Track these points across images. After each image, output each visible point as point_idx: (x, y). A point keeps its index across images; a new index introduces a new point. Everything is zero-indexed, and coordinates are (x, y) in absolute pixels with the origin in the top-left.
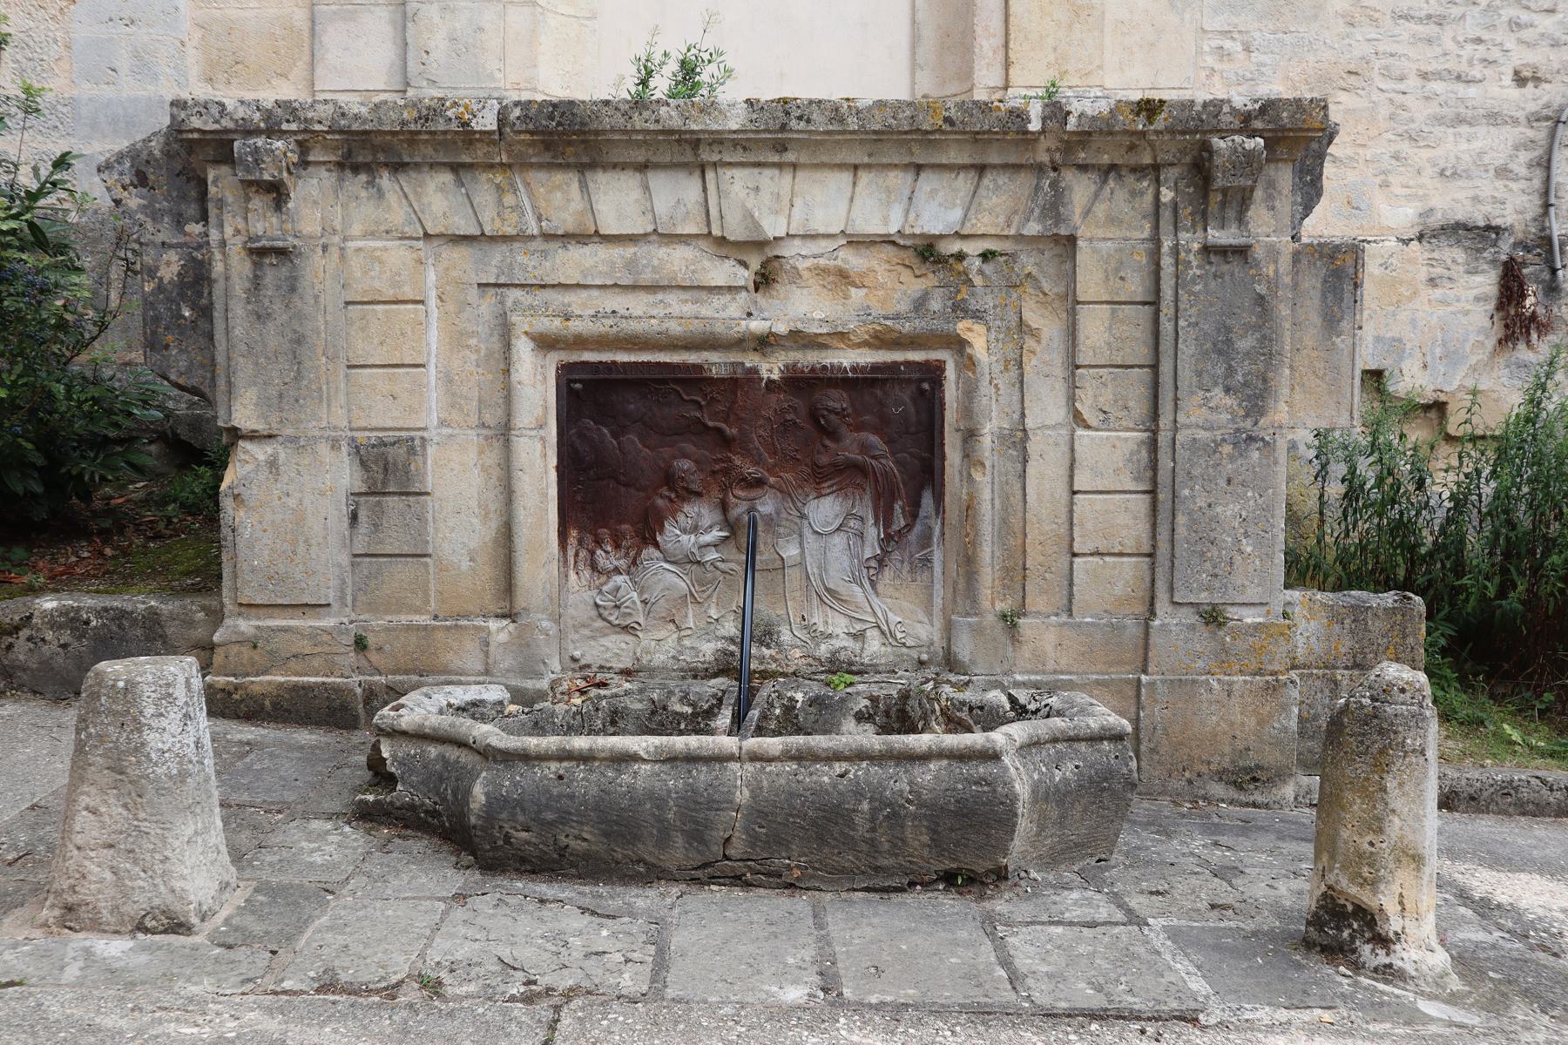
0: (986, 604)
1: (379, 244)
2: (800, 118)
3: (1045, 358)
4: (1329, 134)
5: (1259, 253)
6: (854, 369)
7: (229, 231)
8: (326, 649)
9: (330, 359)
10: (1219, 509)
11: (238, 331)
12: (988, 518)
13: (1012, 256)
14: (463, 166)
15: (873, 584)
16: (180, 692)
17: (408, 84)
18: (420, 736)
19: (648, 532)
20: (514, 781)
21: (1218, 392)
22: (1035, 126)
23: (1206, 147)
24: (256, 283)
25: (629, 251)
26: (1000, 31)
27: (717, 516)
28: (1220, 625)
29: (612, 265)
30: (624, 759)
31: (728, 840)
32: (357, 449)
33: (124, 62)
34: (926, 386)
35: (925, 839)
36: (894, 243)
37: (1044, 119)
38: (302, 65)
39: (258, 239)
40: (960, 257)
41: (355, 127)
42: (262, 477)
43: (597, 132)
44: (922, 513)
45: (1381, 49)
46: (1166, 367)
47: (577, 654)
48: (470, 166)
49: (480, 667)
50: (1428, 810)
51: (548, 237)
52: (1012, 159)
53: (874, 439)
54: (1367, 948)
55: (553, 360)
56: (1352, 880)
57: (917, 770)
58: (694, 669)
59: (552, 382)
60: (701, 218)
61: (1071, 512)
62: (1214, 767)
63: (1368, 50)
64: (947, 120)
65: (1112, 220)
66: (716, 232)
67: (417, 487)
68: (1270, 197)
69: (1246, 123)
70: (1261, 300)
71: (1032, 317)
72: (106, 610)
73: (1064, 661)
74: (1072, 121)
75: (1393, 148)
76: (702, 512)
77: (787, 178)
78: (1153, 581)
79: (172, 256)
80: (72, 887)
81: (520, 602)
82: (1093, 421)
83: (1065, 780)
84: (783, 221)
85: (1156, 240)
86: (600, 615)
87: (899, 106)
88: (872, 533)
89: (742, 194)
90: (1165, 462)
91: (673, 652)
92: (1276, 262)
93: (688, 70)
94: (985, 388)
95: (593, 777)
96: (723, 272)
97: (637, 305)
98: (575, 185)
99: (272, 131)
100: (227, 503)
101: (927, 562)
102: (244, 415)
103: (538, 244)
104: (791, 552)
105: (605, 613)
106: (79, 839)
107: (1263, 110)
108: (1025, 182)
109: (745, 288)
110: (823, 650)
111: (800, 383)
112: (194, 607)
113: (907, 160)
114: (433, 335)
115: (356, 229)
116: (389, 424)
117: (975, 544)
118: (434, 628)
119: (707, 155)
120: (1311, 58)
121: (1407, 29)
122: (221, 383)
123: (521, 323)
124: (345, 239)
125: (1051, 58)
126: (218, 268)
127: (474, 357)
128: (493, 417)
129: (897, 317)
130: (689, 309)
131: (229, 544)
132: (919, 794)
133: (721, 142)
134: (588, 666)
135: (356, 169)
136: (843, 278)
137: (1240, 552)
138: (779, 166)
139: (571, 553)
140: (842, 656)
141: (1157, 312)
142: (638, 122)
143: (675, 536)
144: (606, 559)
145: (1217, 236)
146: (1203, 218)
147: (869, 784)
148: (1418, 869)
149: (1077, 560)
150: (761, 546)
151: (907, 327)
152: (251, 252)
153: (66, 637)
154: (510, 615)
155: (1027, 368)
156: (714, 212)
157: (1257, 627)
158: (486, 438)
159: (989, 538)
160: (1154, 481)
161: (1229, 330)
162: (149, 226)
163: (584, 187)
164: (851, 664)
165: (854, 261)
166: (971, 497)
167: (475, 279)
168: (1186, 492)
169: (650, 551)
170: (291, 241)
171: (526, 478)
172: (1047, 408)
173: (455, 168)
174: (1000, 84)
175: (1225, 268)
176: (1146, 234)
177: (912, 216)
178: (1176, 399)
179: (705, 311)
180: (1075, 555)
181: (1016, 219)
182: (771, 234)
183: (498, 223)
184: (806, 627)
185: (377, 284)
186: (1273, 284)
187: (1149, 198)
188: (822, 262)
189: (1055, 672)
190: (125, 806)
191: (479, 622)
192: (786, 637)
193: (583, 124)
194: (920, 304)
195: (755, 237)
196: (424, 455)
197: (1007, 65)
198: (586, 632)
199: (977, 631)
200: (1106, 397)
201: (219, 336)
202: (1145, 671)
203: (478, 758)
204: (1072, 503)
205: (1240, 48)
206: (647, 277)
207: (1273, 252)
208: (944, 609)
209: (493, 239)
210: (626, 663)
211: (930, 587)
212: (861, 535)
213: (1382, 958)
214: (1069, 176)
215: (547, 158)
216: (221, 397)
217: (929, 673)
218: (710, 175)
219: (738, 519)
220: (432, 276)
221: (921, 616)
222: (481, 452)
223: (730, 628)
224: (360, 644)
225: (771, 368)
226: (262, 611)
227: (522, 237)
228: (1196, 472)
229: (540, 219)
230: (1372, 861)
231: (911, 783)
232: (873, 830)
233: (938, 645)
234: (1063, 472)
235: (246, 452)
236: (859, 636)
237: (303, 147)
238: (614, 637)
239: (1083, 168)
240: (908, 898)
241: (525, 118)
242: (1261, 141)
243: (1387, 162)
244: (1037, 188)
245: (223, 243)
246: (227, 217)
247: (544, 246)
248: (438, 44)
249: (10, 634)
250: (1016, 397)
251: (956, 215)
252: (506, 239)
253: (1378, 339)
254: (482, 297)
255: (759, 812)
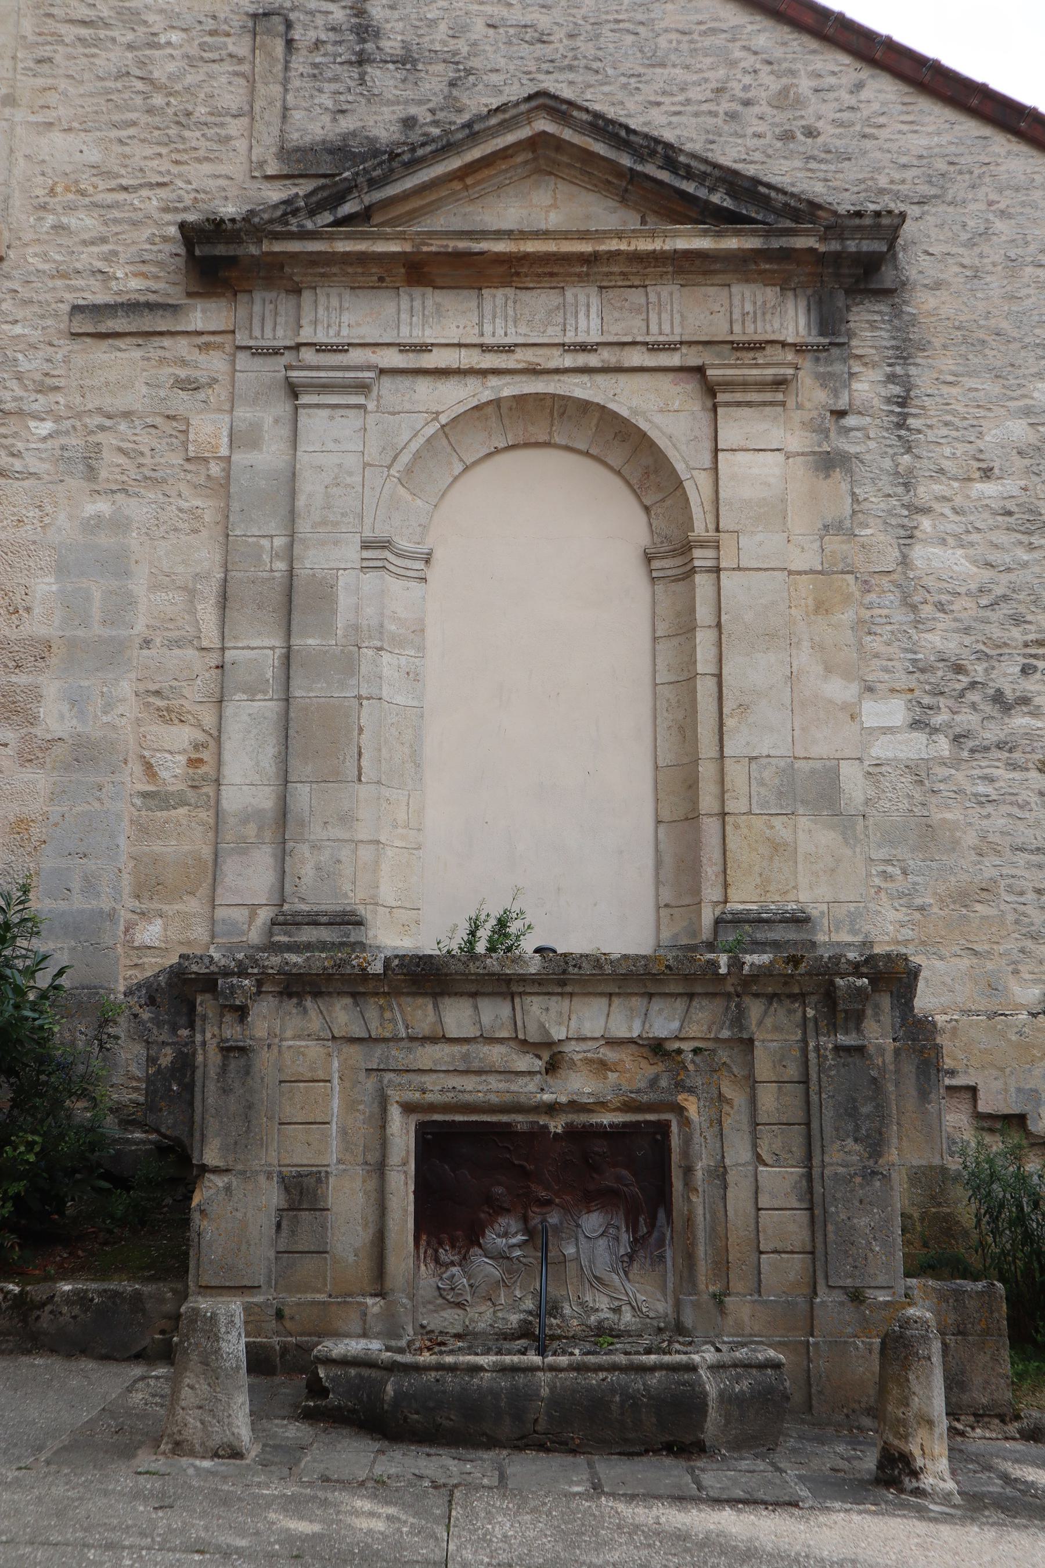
0: (702, 1287)
1: (303, 1043)
2: (575, 966)
3: (736, 1118)
4: (913, 974)
5: (872, 1050)
6: (611, 1125)
7: (208, 1035)
8: (257, 1318)
9: (270, 1119)
10: (855, 1221)
11: (210, 1101)
12: (701, 1226)
13: (714, 1051)
14: (359, 993)
15: (626, 1273)
16: (237, 1320)
17: (284, 901)
18: (345, 1362)
19: (473, 1237)
20: (407, 1383)
21: (850, 1141)
22: (723, 970)
23: (832, 983)
24: (224, 1069)
25: (465, 1048)
26: (720, 861)
27: (520, 1225)
28: (862, 1302)
29: (453, 1056)
30: (477, 1369)
31: (536, 1420)
32: (282, 1179)
33: (76, 885)
34: (659, 1137)
35: (654, 1420)
36: (635, 1043)
37: (729, 966)
38: (206, 885)
39: (228, 1040)
40: (679, 1051)
41: (294, 971)
42: (220, 1198)
43: (446, 975)
44: (658, 1224)
45: (1004, 872)
46: (815, 1125)
47: (425, 1322)
48: (364, 994)
49: (360, 1332)
50: (935, 1393)
51: (412, 1039)
52: (711, 990)
53: (625, 1172)
54: (907, 1479)
55: (413, 1120)
56: (895, 1436)
57: (648, 1376)
58: (505, 1334)
59: (412, 1134)
60: (511, 1027)
61: (757, 1223)
62: (863, 1405)
63: (994, 873)
64: (668, 967)
65: (776, 1029)
66: (521, 1036)
67: (322, 1205)
68: (876, 1014)
69: (856, 969)
70: (874, 1080)
71: (727, 1091)
72: (105, 1291)
73: (756, 1328)
74: (746, 968)
75: (1020, 945)
76: (510, 1223)
77: (566, 1002)
78: (815, 1271)
79: (168, 1050)
80: (180, 1432)
81: (389, 1284)
82: (769, 1161)
83: (742, 1391)
84: (564, 1029)
85: (805, 1041)
86: (441, 1295)
87: (637, 958)
88: (625, 1237)
89: (538, 1013)
90: (818, 1189)
91: (490, 1322)
92: (883, 1055)
93: (502, 923)
94: (697, 1139)
95: (456, 1380)
96: (524, 1062)
97: (469, 1083)
98: (430, 1006)
99: (242, 973)
100: (196, 1216)
101: (662, 1258)
102: (211, 1156)
103: (405, 1044)
104: (570, 1250)
105: (444, 1293)
106: (183, 1404)
107: (867, 961)
108: (718, 1004)
109: (539, 1072)
110: (593, 1319)
111: (576, 1134)
112: (166, 1290)
113: (643, 990)
114: (336, 1103)
115: (289, 1034)
116: (305, 1162)
117: (693, 1244)
118: (330, 1303)
119: (515, 988)
120: (953, 879)
121: (1022, 858)
122: (197, 1135)
123: (394, 1095)
124: (281, 1040)
125: (758, 881)
126: (200, 1058)
127: (362, 1117)
128: (373, 1157)
129: (638, 1091)
130: (502, 1086)
131: (195, 1244)
132: (649, 1391)
133: (525, 980)
134: (432, 1331)
135: (290, 995)
136: (602, 1066)
137: (872, 1250)
138: (561, 994)
139: (422, 1251)
140: (606, 1324)
141: (808, 1088)
142: (472, 968)
143: (493, 1239)
144: (445, 1255)
145: (843, 1039)
146: (833, 1028)
147: (619, 1385)
148: (931, 1429)
149: (763, 1256)
150: (550, 1246)
151: (645, 1098)
152: (222, 1049)
153: (76, 1310)
154: (381, 1294)
155: (725, 1125)
156: (519, 1024)
157: (887, 1304)
158: (368, 1172)
159: (702, 1240)
160: (811, 1201)
161: (854, 1100)
162: (155, 1031)
163: (436, 1007)
164: (612, 1329)
165: (610, 1055)
166: (690, 1212)
167: (364, 1066)
168: (833, 1209)
169: (476, 1250)
170: (249, 1042)
171: (394, 1199)
172: (738, 1152)
173: (354, 995)
174: (721, 899)
175: (850, 1060)
176: (799, 1037)
177: (647, 1026)
178: (823, 1146)
179: (514, 1087)
180: (761, 1253)
181: (714, 1028)
182: (556, 1038)
183: (380, 1030)
184: (581, 1304)
185: (301, 1069)
186: (883, 1070)
187: (799, 1014)
188: (589, 1055)
189: (751, 1335)
190: (209, 1384)
191: (360, 1299)
192: (567, 1311)
193: (438, 969)
194: (653, 1083)
195: (545, 1040)
196: (327, 1183)
197: (726, 886)
198: (431, 1307)
199: (696, 1305)
200: (777, 1146)
201: (198, 1103)
202: (812, 1336)
203: (384, 1372)
204: (758, 1217)
205: (899, 872)
206: (476, 1065)
207: (881, 1050)
208: (674, 1292)
209: (377, 1040)
210: (458, 1329)
211: (664, 1276)
212: (617, 1239)
213: (915, 1484)
214: (747, 1000)
215: (414, 989)
216: (196, 1145)
217: (666, 1336)
218: (517, 1000)
219: (535, 1227)
220: (336, 1064)
221: (659, 1296)
222: (364, 1182)
223: (529, 1304)
224: (279, 1315)
225: (556, 1125)
226: (214, 1291)
227: (395, 1039)
228: (838, 1195)
229: (407, 1028)
230: (903, 1423)
231: (644, 1384)
232: (622, 1414)
233: (671, 1316)
234: (751, 1195)
235: (210, 1181)
236: (617, 1310)
237: (259, 983)
238: (449, 1311)
239: (756, 995)
240: (645, 1459)
241: (401, 966)
242: (866, 980)
243: (1016, 956)
244: (728, 1008)
245: (204, 1043)
246: (208, 1027)
247: (410, 1045)
248: (308, 871)
249: (39, 1308)
250: (718, 1145)
251: (676, 1025)
252: (385, 1040)
253: (1019, 1090)
254: (368, 1077)
255: (556, 1401)
